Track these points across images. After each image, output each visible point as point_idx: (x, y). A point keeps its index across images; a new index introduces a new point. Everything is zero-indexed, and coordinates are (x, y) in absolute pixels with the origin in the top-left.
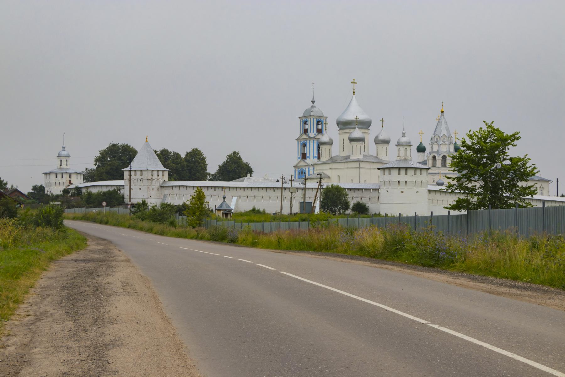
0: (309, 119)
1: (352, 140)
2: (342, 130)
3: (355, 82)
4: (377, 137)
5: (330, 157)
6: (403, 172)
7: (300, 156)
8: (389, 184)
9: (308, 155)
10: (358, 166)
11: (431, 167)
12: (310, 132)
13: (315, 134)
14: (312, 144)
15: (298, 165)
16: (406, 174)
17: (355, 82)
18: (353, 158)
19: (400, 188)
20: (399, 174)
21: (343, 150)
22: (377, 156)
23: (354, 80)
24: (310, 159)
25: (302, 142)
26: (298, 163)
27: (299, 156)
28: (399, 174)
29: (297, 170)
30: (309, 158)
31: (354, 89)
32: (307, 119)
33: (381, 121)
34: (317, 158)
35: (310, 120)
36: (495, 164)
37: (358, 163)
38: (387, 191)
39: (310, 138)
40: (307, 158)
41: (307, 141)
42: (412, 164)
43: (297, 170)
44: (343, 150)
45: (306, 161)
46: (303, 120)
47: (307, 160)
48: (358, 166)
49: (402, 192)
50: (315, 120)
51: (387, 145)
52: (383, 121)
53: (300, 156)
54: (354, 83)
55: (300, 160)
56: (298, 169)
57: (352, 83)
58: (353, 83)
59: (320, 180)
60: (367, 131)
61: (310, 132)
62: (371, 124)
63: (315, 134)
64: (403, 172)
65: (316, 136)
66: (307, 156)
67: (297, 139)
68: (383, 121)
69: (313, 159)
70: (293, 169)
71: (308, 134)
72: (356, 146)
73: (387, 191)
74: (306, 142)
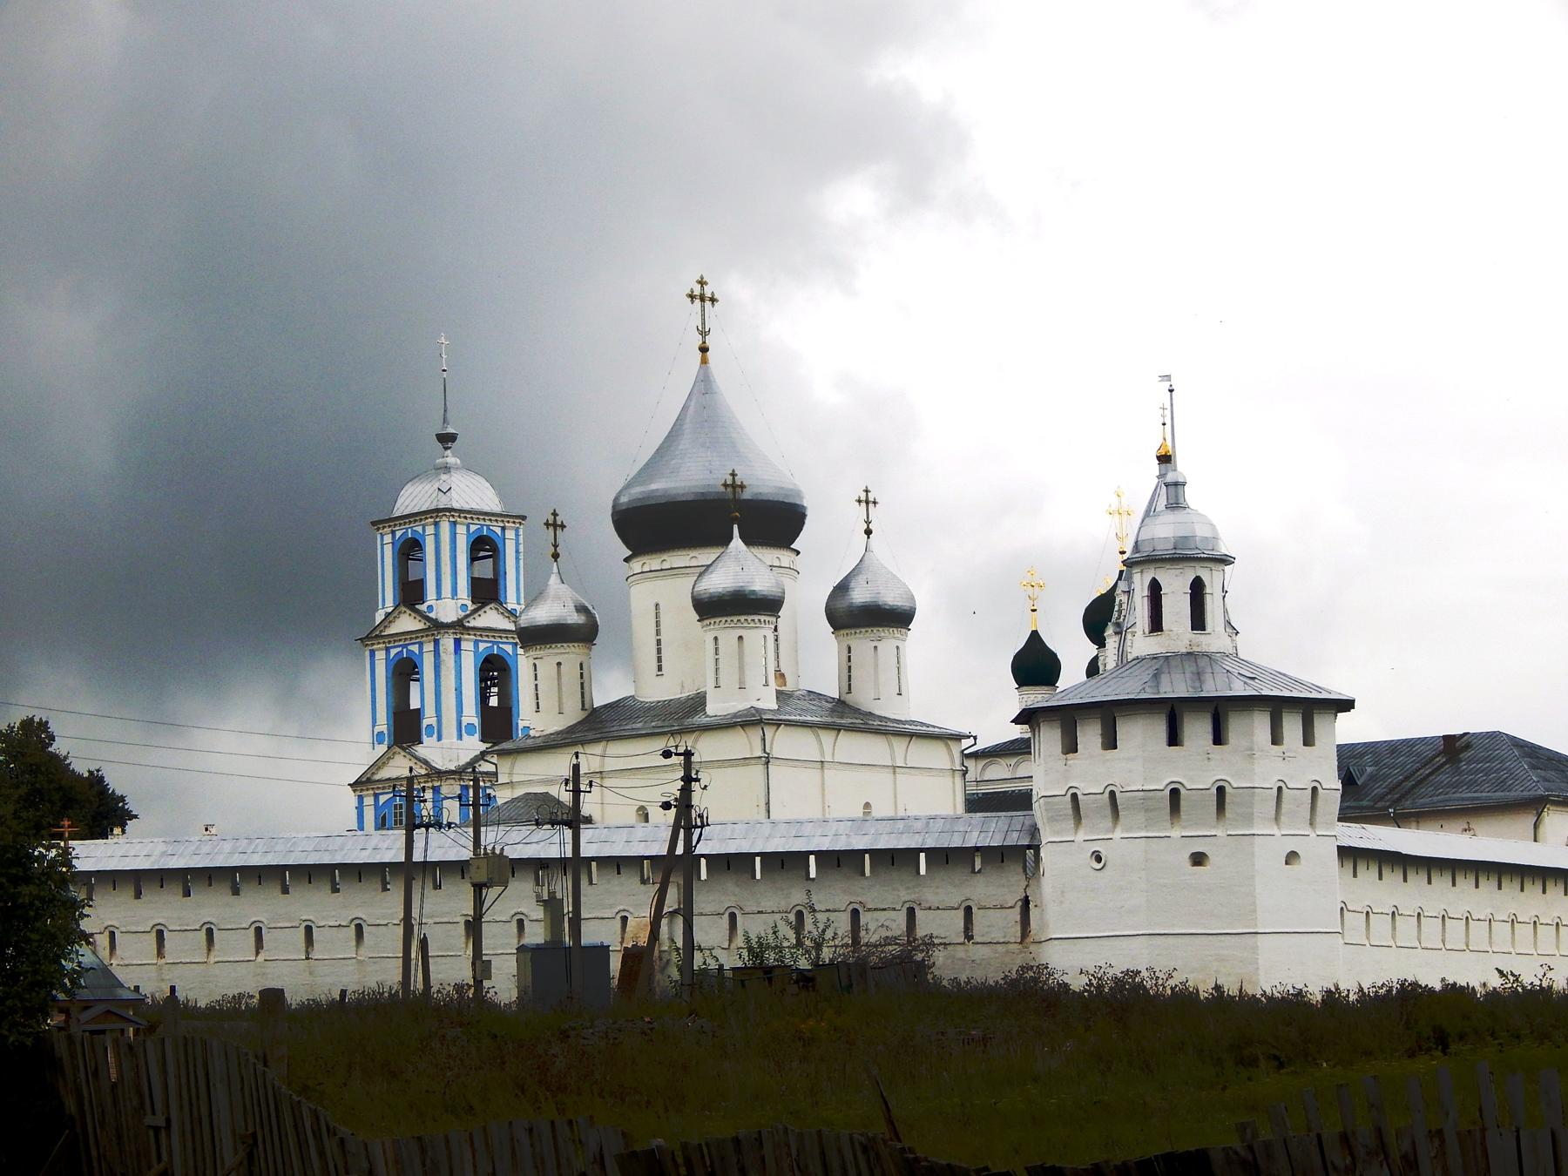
0: (430, 530)
1: (710, 608)
2: (645, 559)
3: (708, 295)
4: (842, 588)
5: (583, 708)
6: (1197, 730)
7: (383, 725)
8: (1108, 811)
9: (428, 719)
10: (759, 753)
11: (519, 941)
12: (439, 598)
13: (464, 606)
14: (448, 659)
15: (377, 777)
16: (1218, 739)
17: (708, 295)
18: (716, 707)
19: (1179, 838)
20: (1174, 739)
21: (660, 668)
22: (848, 698)
23: (702, 283)
24: (439, 739)
25: (393, 652)
26: (378, 765)
27: (377, 729)
28: (1174, 739)
29: (369, 801)
30: (435, 736)
31: (704, 333)
32: (419, 529)
33: (859, 501)
34: (477, 736)
35: (437, 535)
36: (504, 985)
37: (755, 734)
38: (1099, 859)
39: (437, 626)
40: (425, 738)
41: (421, 645)
42: (1253, 679)
43: (369, 801)
44: (660, 668)
45: (420, 750)
46: (398, 534)
47: (429, 749)
48: (759, 753)
49: (1198, 859)
50: (461, 529)
51: (896, 632)
52: (867, 502)
53: (384, 728)
54: (702, 299)
55: (383, 748)
56: (376, 796)
57: (692, 297)
58: (697, 302)
59: (682, 790)
60: (784, 557)
61: (439, 598)
62: (597, 630)
63: (464, 606)
64: (1197, 730)
65: (467, 616)
66: (425, 723)
67: (367, 637)
68: (867, 502)
69: (460, 737)
70: (351, 798)
71: (423, 607)
72: (740, 638)
73: (1099, 859)
74: (415, 648)
